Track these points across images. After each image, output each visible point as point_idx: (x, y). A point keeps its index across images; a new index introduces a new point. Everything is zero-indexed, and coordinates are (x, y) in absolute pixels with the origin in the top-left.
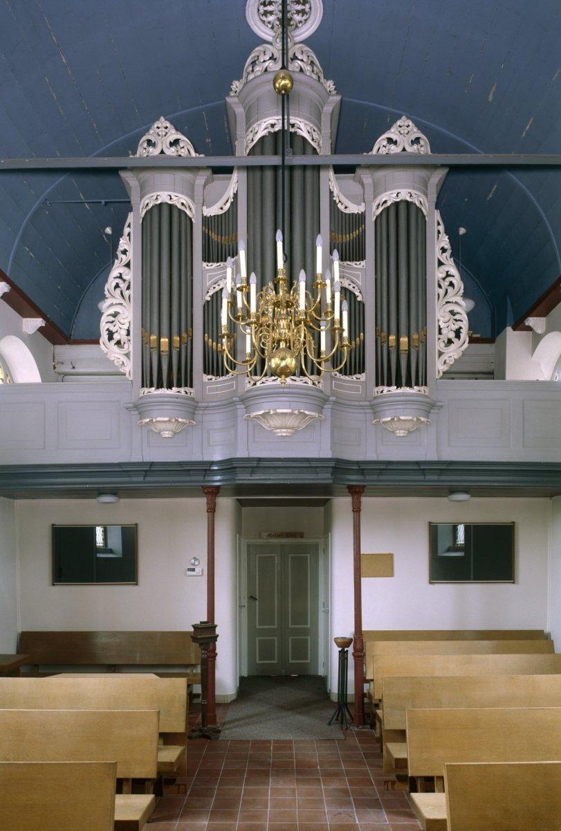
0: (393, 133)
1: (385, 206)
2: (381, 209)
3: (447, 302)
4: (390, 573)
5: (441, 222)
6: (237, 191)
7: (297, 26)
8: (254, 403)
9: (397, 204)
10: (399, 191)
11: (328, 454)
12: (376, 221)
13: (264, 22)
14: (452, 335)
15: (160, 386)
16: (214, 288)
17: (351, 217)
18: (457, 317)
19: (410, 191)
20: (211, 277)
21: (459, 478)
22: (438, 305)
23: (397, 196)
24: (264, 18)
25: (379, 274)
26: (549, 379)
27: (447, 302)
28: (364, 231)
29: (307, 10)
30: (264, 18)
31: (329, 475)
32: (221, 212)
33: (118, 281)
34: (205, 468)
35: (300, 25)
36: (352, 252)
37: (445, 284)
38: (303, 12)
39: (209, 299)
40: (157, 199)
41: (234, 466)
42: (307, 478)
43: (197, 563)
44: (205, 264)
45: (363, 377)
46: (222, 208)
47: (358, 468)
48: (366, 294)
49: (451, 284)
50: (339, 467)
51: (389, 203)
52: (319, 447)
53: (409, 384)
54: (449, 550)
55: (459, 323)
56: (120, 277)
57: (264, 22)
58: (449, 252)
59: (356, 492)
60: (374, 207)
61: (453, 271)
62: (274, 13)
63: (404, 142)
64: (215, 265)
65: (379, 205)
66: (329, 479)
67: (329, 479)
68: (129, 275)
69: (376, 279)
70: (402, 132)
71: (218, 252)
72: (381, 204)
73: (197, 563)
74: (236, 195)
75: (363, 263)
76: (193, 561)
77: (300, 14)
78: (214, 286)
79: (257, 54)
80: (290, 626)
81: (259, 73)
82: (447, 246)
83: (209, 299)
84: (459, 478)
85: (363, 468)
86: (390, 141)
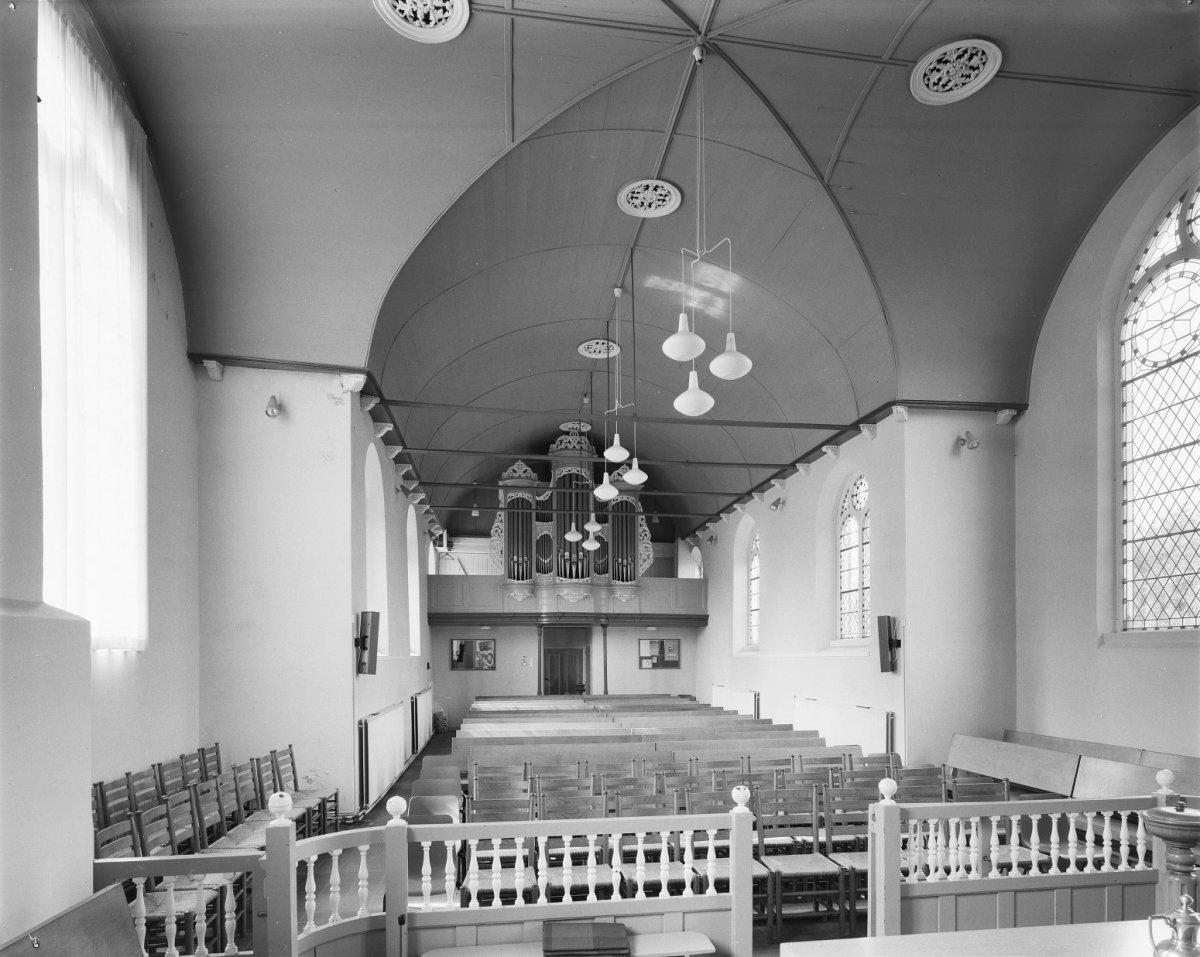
0: (515, 467)
4: (884, 669)
9: (622, 502)
11: (593, 611)
15: (518, 579)
17: (624, 505)
34: (538, 616)
36: (601, 520)
37: (643, 535)
42: (584, 621)
45: (607, 575)
48: (608, 539)
50: (597, 617)
52: (588, 608)
53: (523, 579)
54: (743, 650)
59: (604, 626)
61: (647, 529)
63: (520, 472)
68: (502, 526)
85: (608, 616)
86: (514, 471)
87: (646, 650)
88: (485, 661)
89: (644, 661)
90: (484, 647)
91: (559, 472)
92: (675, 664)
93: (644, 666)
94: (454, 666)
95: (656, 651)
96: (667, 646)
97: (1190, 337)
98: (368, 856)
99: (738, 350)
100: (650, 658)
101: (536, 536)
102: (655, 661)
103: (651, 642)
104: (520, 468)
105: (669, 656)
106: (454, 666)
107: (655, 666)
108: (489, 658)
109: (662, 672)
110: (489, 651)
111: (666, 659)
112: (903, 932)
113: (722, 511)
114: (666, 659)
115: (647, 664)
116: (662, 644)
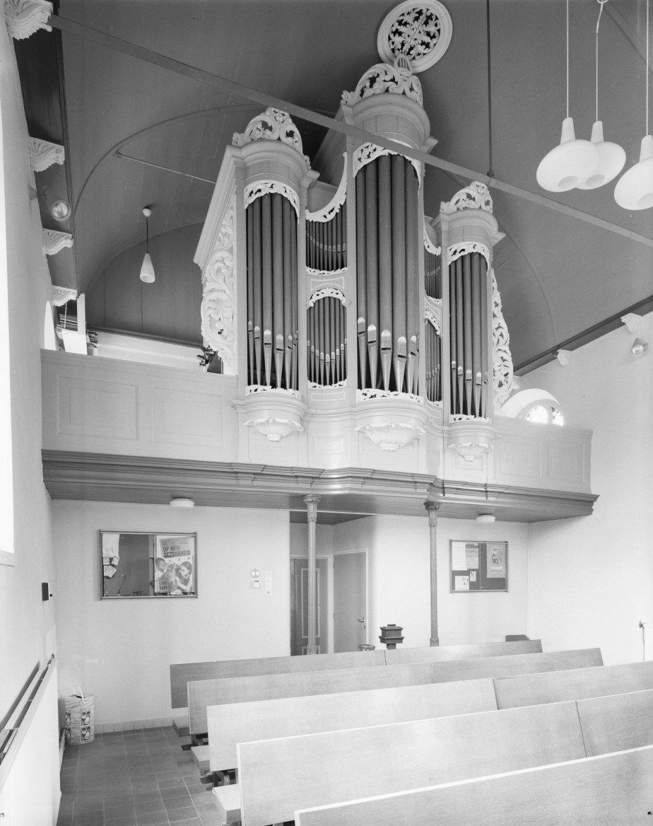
1: (259, 195)
2: (254, 197)
3: (499, 350)
5: (495, 280)
6: (345, 203)
7: (414, 58)
8: (256, 409)
10: (274, 182)
12: (247, 210)
13: (390, 39)
14: (502, 379)
16: (318, 295)
18: (505, 363)
19: (285, 185)
20: (315, 284)
21: (470, 497)
22: (495, 349)
23: (474, 247)
24: (392, 36)
25: (454, 313)
26: (546, 422)
27: (499, 350)
28: (440, 272)
29: (431, 45)
30: (392, 36)
31: (425, 491)
32: (324, 220)
33: (221, 265)
35: (417, 58)
38: (427, 45)
39: (312, 305)
40: (272, 187)
41: (416, 480)
43: (258, 574)
44: (308, 269)
46: (325, 216)
47: (484, 490)
49: (501, 335)
51: (262, 194)
55: (508, 369)
56: (223, 261)
57: (390, 39)
58: (500, 307)
60: (247, 194)
61: (504, 324)
62: (403, 35)
64: (318, 271)
65: (252, 192)
66: (424, 494)
67: (424, 494)
69: (450, 318)
70: (479, 191)
71: (325, 261)
72: (254, 192)
73: (253, 574)
74: (343, 208)
75: (440, 301)
76: (253, 574)
77: (424, 47)
78: (318, 293)
79: (378, 71)
80: (303, 637)
81: (378, 91)
82: (499, 302)
83: (312, 305)
84: (470, 497)
86: (469, 196)
87: (463, 559)
88: (173, 578)
89: (458, 579)
90: (170, 551)
91: (357, 158)
92: (500, 584)
93: (457, 588)
94: (106, 588)
95: (475, 564)
96: (490, 552)
97: (423, 494)
98: (493, 266)
99: (495, 248)
100: (467, 573)
101: (306, 302)
102: (473, 578)
103: (467, 546)
104: (280, 121)
105: (494, 571)
106: (106, 588)
107: (474, 587)
108: (185, 571)
109: (485, 598)
110: (184, 559)
111: (489, 576)
112: (45, 453)
113: (559, 347)
114: (489, 576)
115: (462, 583)
116: (483, 548)
